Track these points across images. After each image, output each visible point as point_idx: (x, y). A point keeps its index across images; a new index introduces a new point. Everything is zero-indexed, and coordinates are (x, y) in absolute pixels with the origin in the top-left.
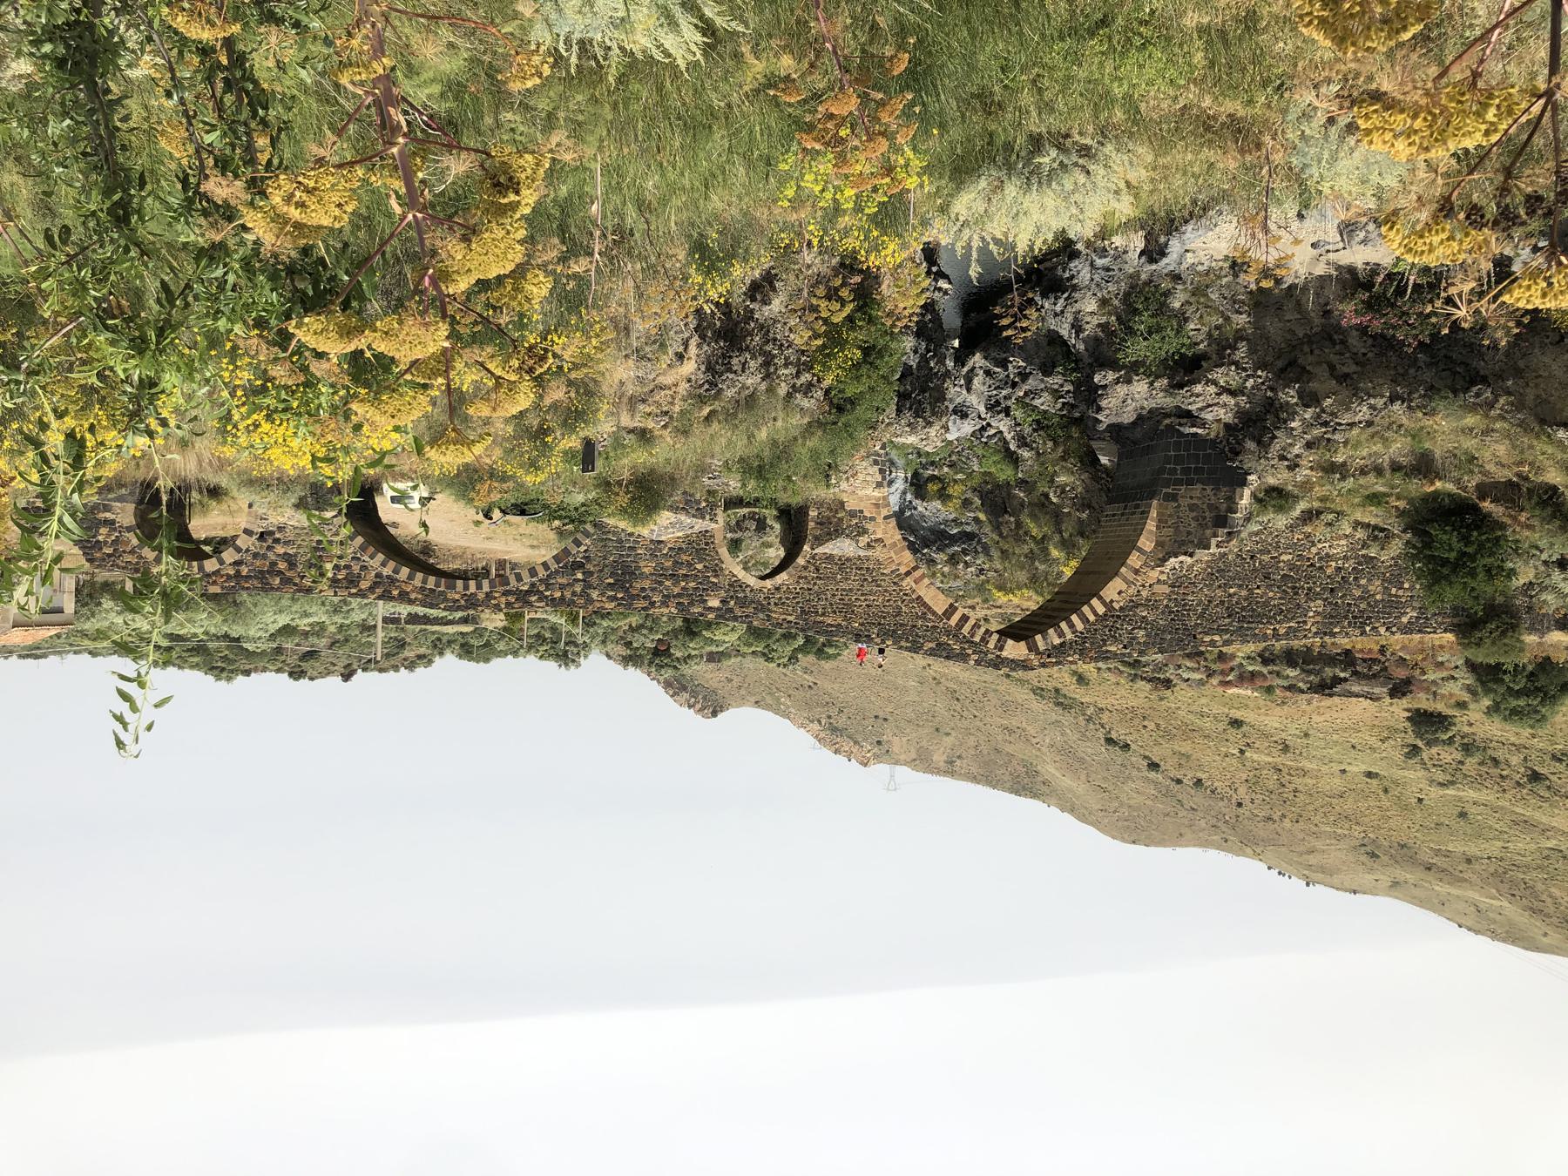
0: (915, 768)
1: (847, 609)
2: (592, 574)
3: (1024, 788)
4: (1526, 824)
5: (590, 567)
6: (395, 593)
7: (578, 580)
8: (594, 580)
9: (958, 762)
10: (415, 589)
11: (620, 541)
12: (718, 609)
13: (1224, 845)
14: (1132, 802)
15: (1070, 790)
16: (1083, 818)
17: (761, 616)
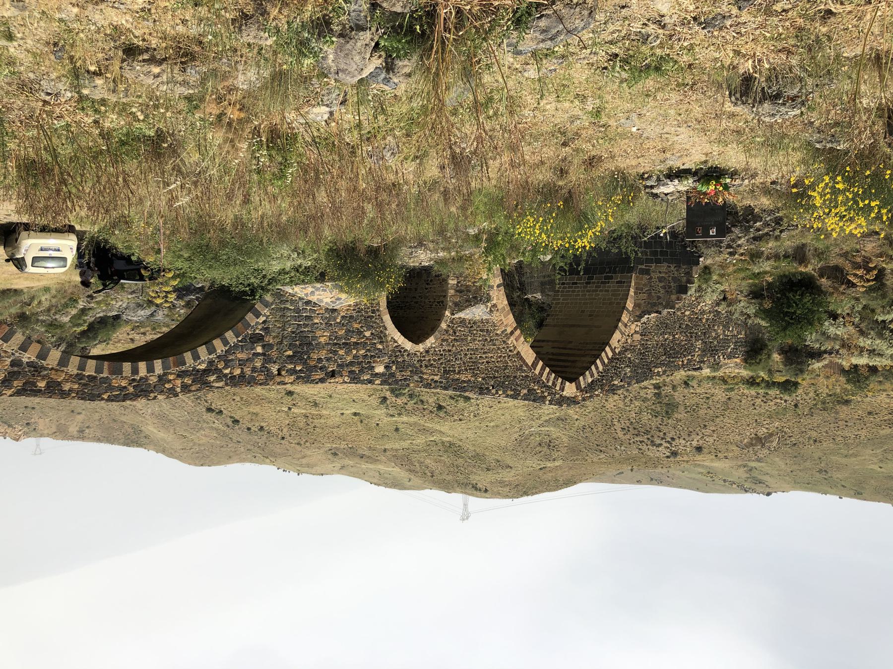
0: (56, 438)
1: (473, 367)
2: (271, 346)
3: (133, 442)
4: (424, 430)
5: (269, 339)
6: (42, 384)
7: (258, 354)
8: (274, 353)
9: (87, 431)
10: (70, 378)
11: (297, 311)
12: (383, 375)
13: (254, 459)
14: (201, 442)
15: (163, 439)
16: (170, 455)
17: (416, 378)
